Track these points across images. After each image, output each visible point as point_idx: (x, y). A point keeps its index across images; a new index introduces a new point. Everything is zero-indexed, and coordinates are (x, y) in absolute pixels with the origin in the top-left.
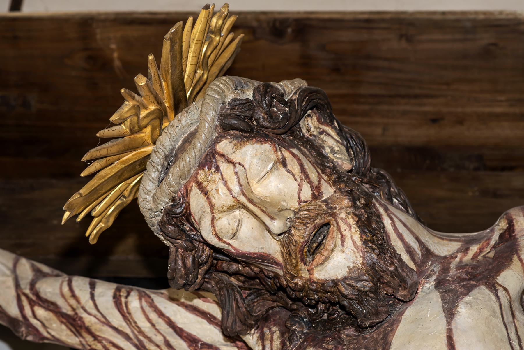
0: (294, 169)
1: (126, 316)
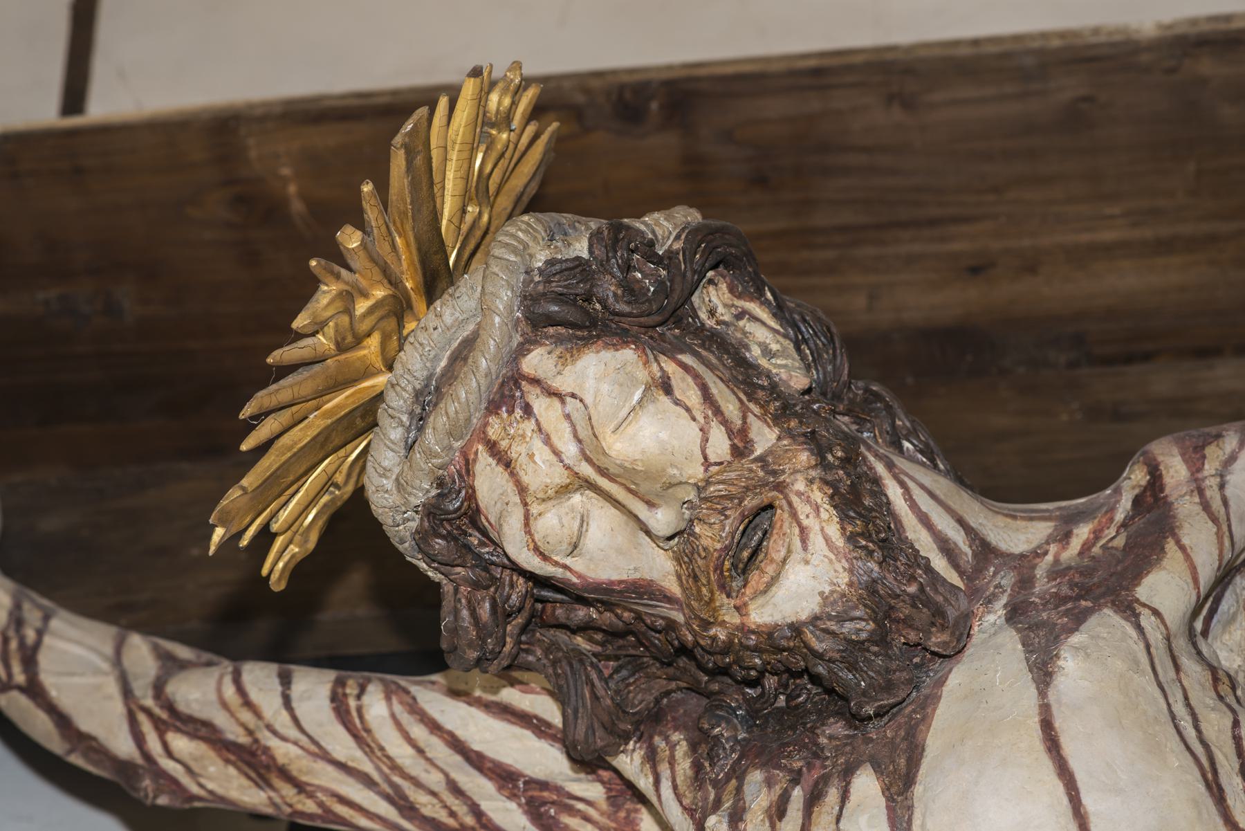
0: (688, 398)
1: (361, 736)
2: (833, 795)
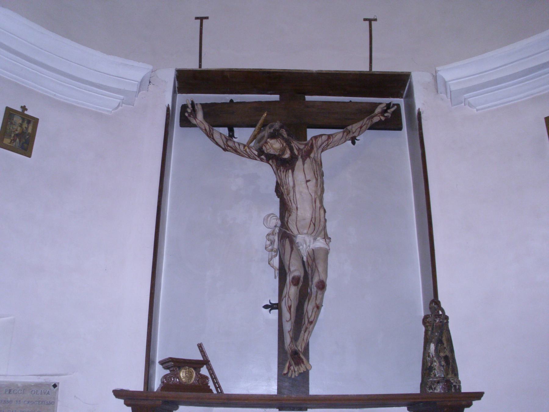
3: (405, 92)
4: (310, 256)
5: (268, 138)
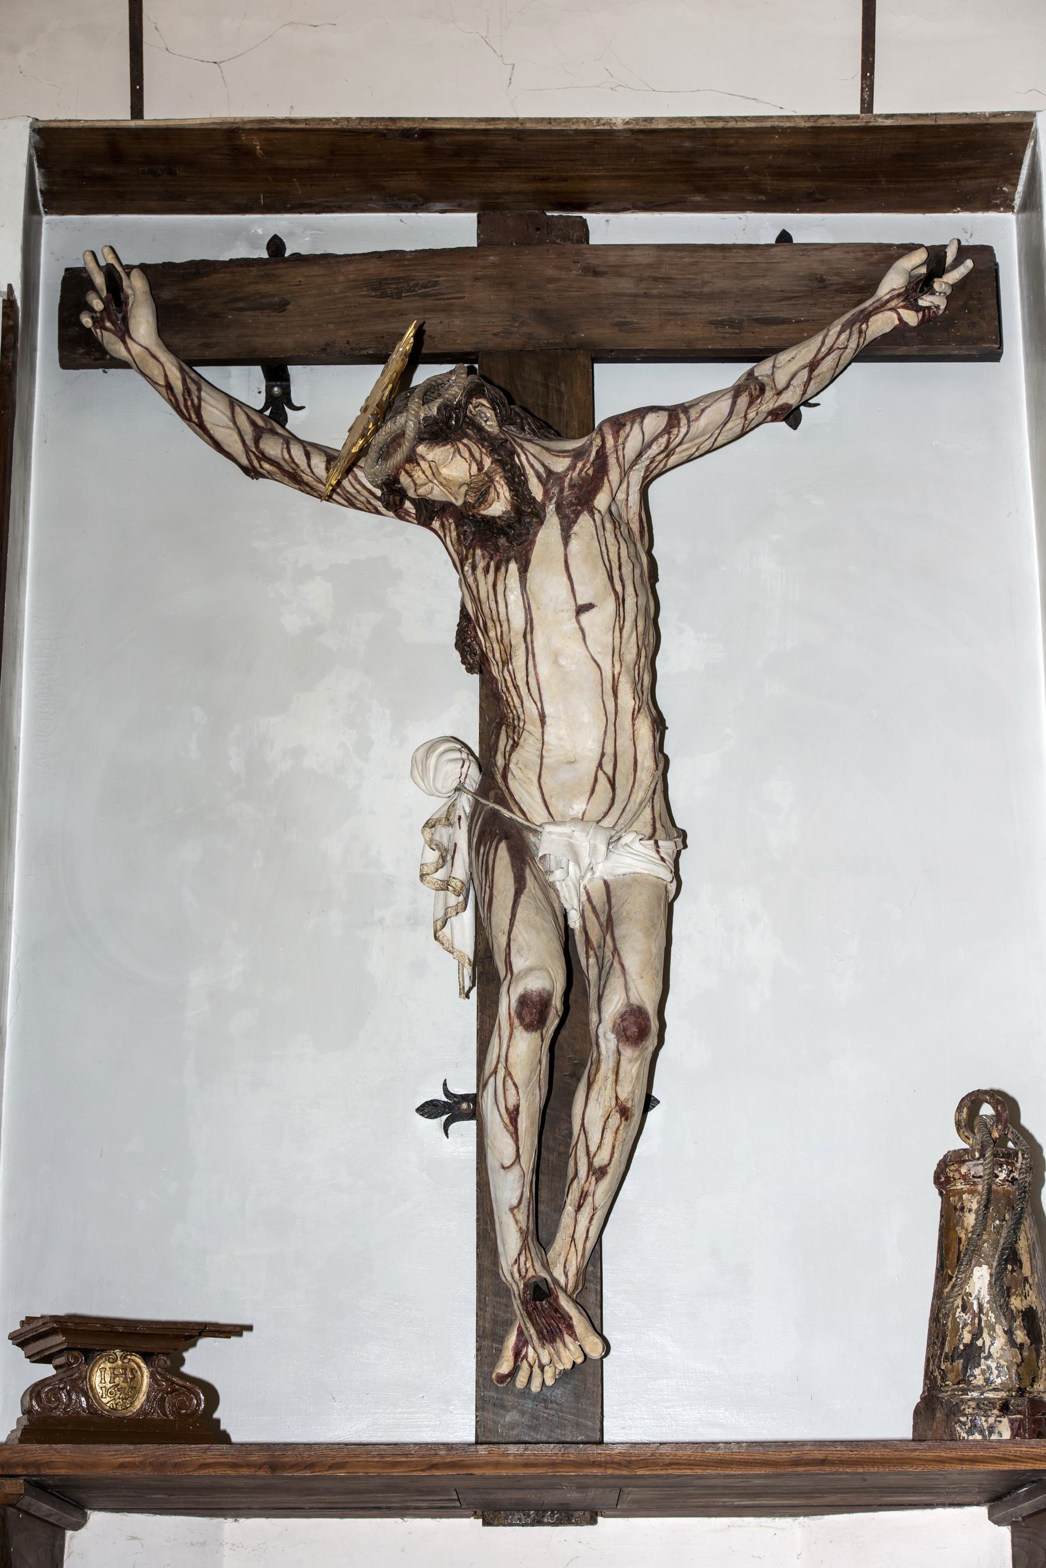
2: (503, 569)
3: (1020, 188)
4: (594, 908)
5: (420, 440)
